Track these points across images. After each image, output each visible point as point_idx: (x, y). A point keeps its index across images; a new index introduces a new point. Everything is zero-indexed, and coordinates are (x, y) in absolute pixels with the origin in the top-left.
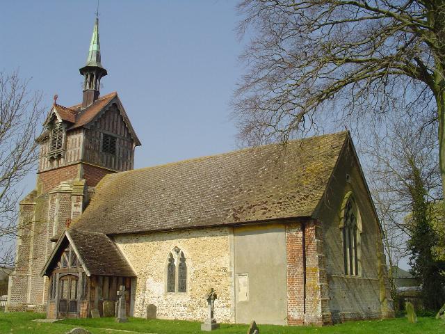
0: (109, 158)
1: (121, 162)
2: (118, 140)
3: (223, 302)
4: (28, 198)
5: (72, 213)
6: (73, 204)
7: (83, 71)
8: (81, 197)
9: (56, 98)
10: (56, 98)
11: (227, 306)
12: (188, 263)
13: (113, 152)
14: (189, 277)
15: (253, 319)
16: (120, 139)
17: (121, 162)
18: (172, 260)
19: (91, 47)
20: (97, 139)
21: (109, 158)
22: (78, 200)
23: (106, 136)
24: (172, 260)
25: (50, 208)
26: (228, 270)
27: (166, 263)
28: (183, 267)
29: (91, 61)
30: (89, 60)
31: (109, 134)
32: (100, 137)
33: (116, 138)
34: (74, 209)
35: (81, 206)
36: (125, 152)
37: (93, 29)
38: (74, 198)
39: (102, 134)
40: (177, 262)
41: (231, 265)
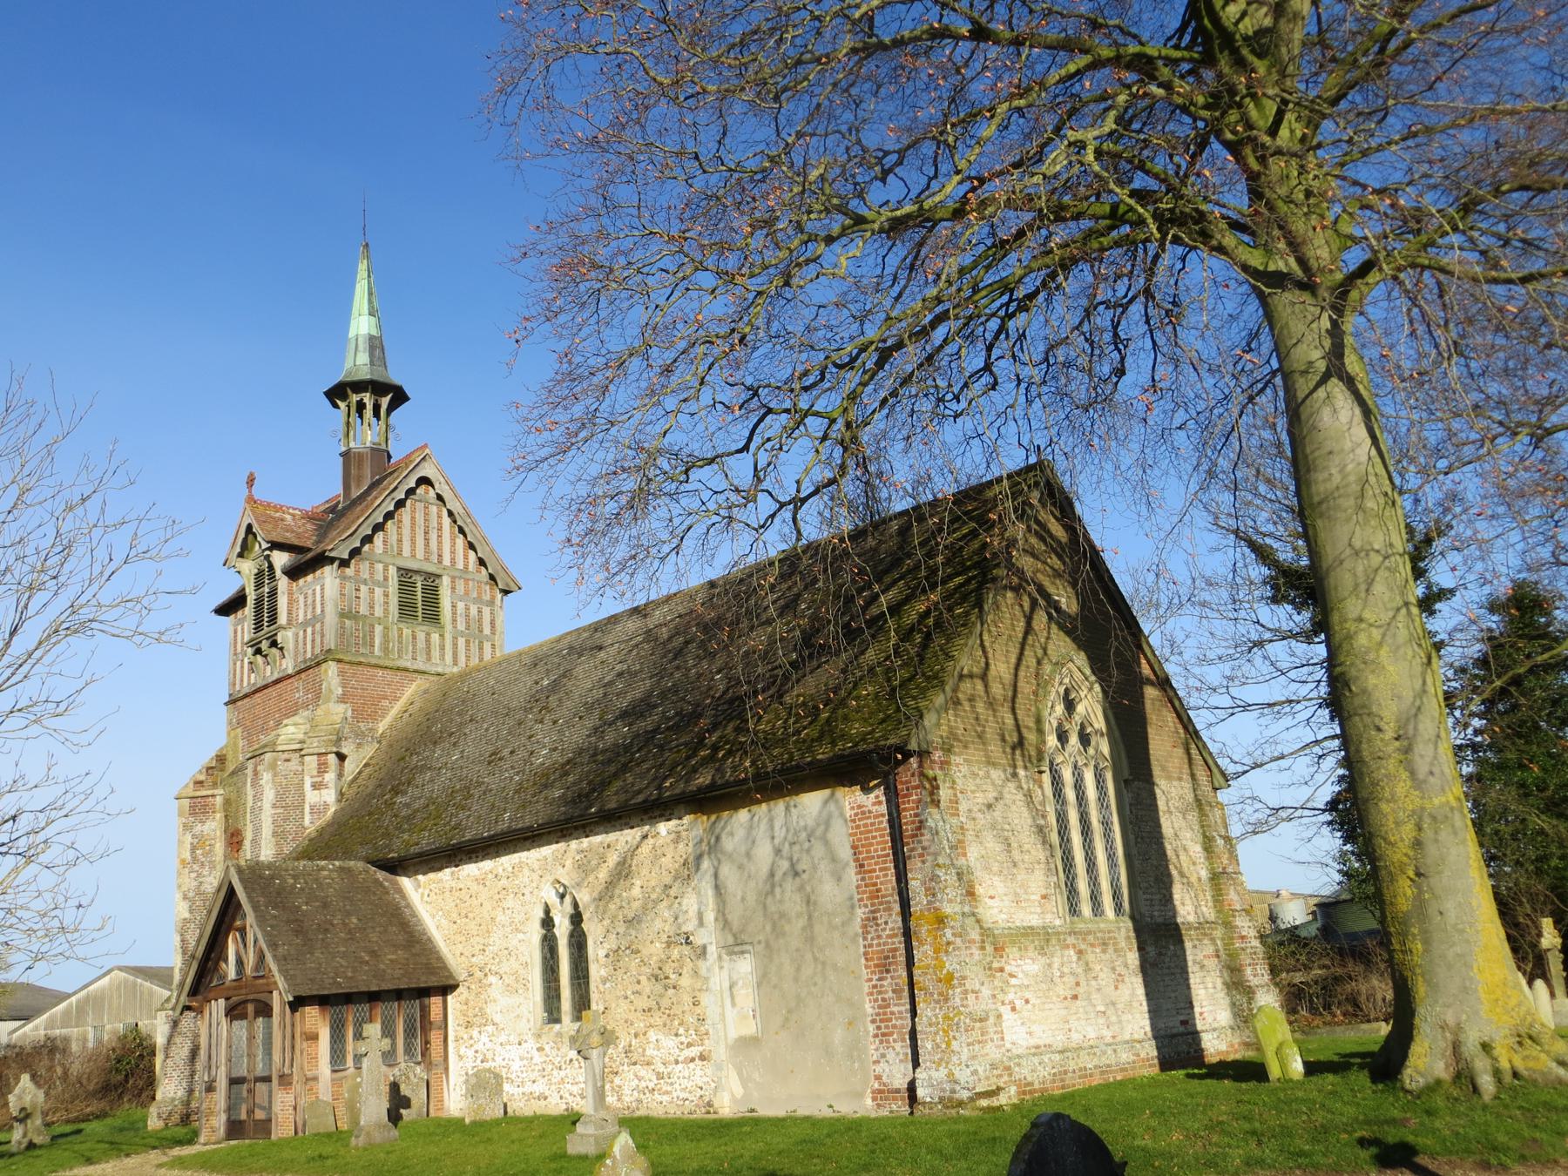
0: (421, 636)
1: (461, 642)
2: (446, 581)
3: (689, 1045)
4: (202, 778)
5: (307, 810)
6: (308, 782)
7: (336, 394)
8: (332, 759)
9: (251, 481)
10: (251, 481)
11: (702, 1058)
12: (591, 927)
13: (432, 614)
14: (596, 971)
15: (131, 1021)
16: (453, 579)
17: (461, 642)
18: (548, 923)
19: (353, 324)
20: (379, 584)
21: (421, 636)
22: (322, 768)
23: (404, 572)
24: (548, 923)
25: (250, 799)
26: (698, 940)
27: (536, 933)
28: (578, 942)
29: (358, 364)
30: (348, 364)
31: (414, 565)
32: (386, 579)
33: (439, 576)
34: (311, 797)
35: (332, 785)
36: (474, 610)
37: (355, 273)
38: (311, 762)
39: (392, 571)
40: (562, 928)
41: (701, 923)
